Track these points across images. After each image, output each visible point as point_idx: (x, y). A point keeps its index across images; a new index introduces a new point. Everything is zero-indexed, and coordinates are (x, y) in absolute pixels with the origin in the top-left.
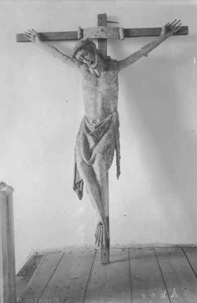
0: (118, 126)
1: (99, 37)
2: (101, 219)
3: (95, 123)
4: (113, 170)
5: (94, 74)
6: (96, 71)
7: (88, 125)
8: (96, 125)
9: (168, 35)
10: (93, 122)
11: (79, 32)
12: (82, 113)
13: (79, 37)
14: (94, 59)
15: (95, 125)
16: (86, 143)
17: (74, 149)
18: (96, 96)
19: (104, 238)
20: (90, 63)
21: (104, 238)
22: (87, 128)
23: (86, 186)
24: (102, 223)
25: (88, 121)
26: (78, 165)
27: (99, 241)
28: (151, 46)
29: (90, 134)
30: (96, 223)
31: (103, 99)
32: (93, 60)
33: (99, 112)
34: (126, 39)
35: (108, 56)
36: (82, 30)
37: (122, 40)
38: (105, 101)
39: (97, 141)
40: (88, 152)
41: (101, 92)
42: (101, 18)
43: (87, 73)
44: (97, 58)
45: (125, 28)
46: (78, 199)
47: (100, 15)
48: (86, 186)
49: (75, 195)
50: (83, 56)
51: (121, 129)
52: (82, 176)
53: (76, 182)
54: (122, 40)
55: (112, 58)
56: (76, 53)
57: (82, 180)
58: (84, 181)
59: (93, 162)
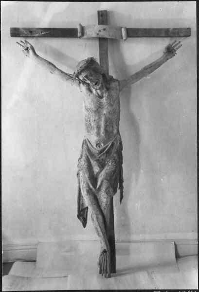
0: (122, 149)
1: (100, 36)
2: (105, 246)
3: (99, 147)
4: (116, 198)
5: (97, 95)
6: (98, 91)
7: (92, 149)
8: (100, 149)
9: (168, 57)
10: (97, 146)
11: (79, 30)
12: (83, 135)
13: (79, 35)
14: (98, 80)
15: (99, 149)
16: (90, 167)
17: (76, 173)
18: (100, 118)
19: (106, 150)
20: (94, 84)
21: (106, 150)
22: (89, 150)
23: (91, 213)
24: (107, 250)
25: (90, 144)
26: (84, 193)
27: (104, 270)
28: (152, 68)
29: (95, 159)
30: (98, 252)
31: (106, 121)
32: (97, 81)
33: (102, 134)
34: (129, 39)
35: (110, 76)
36: (83, 28)
37: (125, 40)
38: (108, 124)
39: (102, 166)
40: (93, 179)
41: (105, 114)
42: (102, 16)
43: (89, 93)
44: (101, 80)
45: (128, 27)
46: (83, 227)
47: (101, 11)
48: (91, 213)
49: (79, 223)
50: (86, 77)
51: (125, 153)
52: (87, 201)
53: (81, 210)
54: (125, 40)
55: (114, 78)
56: (79, 73)
57: (87, 208)
58: (89, 207)
59: (99, 189)
